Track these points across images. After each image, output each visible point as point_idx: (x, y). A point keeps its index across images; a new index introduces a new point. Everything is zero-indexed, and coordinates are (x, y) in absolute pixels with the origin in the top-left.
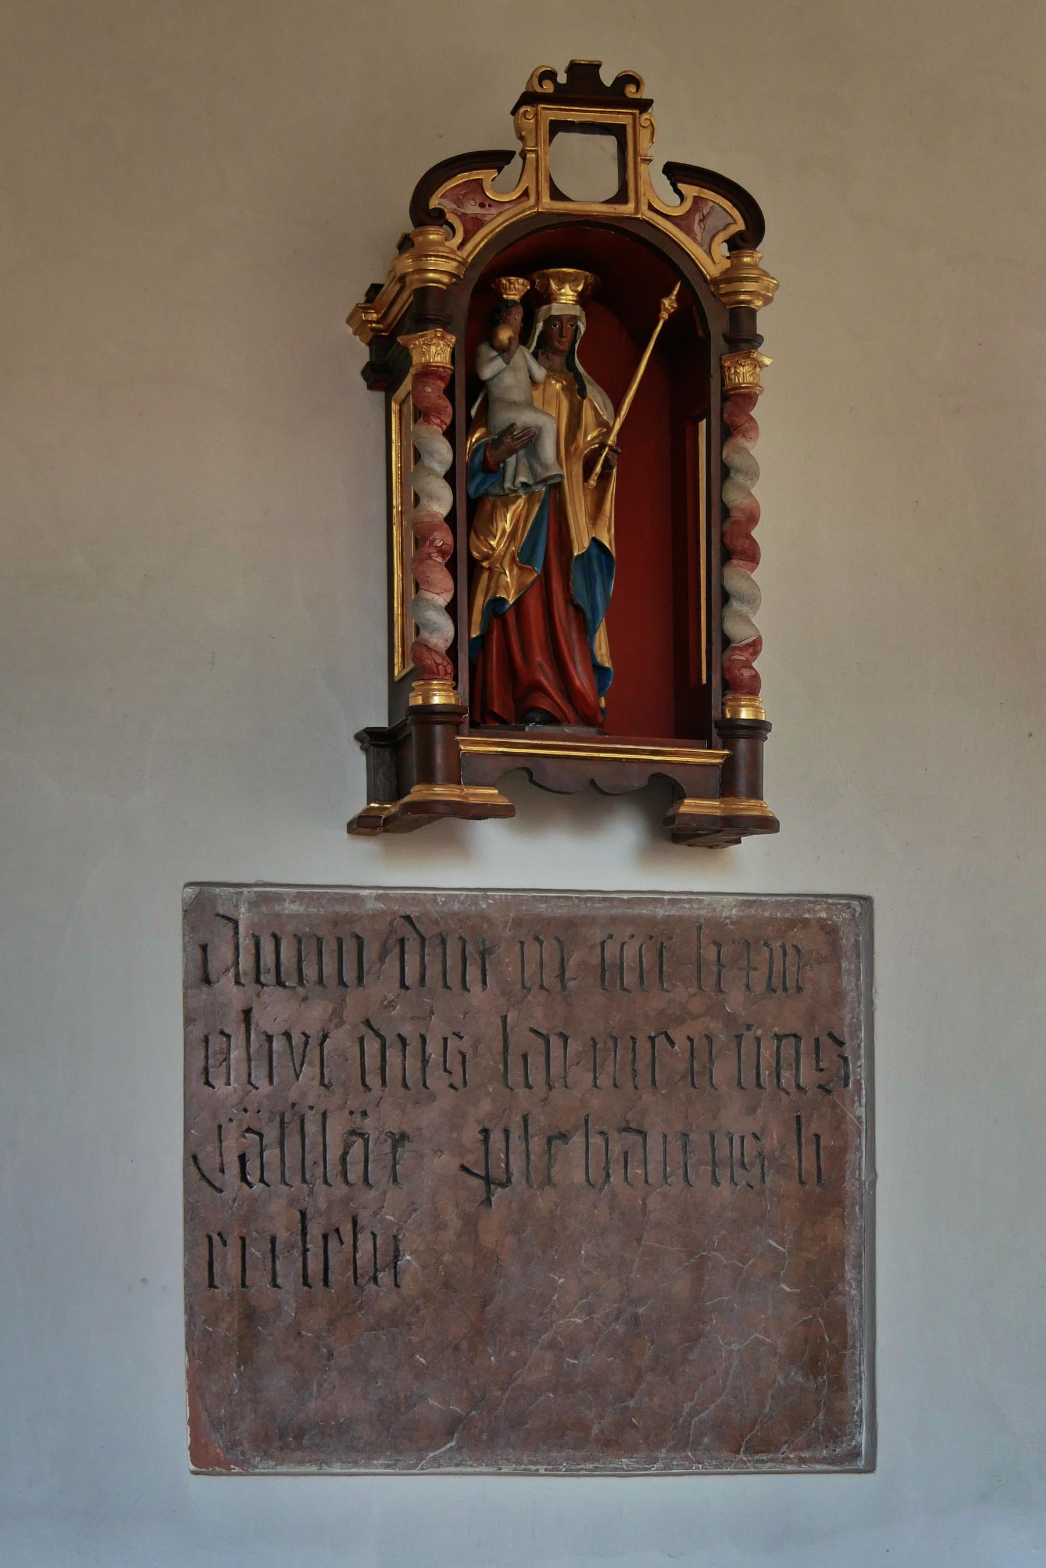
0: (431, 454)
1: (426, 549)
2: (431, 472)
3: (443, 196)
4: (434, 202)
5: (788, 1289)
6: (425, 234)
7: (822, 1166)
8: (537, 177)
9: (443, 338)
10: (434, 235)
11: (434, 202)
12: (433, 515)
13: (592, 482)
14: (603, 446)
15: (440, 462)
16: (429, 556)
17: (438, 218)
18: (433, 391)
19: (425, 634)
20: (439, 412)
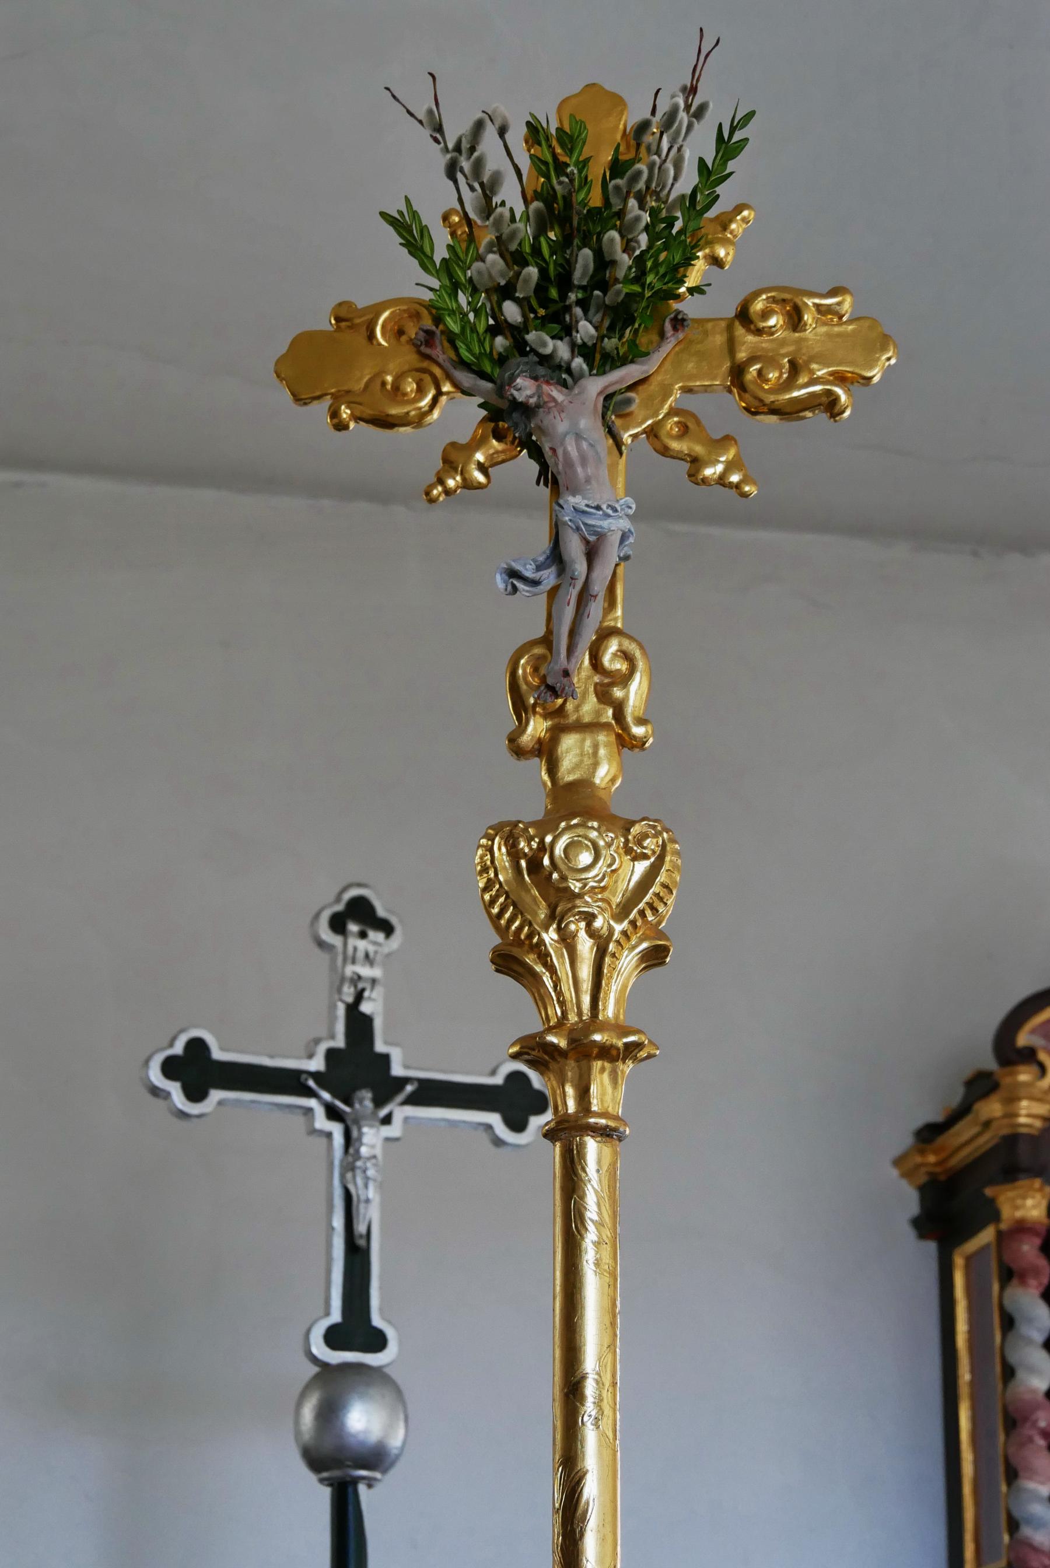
0: (1030, 1321)
1: (1027, 1431)
2: (1030, 1341)
3: (1033, 1031)
4: (1023, 1039)
5: (513, 928)
6: (1014, 1074)
7: (590, 1362)
8: (671, 189)
9: (1041, 1190)
10: (1024, 1076)
11: (1023, 1039)
12: (1034, 1391)
13: (543, 143)
14: (582, 754)
15: (1039, 1330)
16: (1030, 1440)
17: (1029, 1056)
18: (1029, 1249)
19: (1026, 1531)
20: (1036, 1272)
